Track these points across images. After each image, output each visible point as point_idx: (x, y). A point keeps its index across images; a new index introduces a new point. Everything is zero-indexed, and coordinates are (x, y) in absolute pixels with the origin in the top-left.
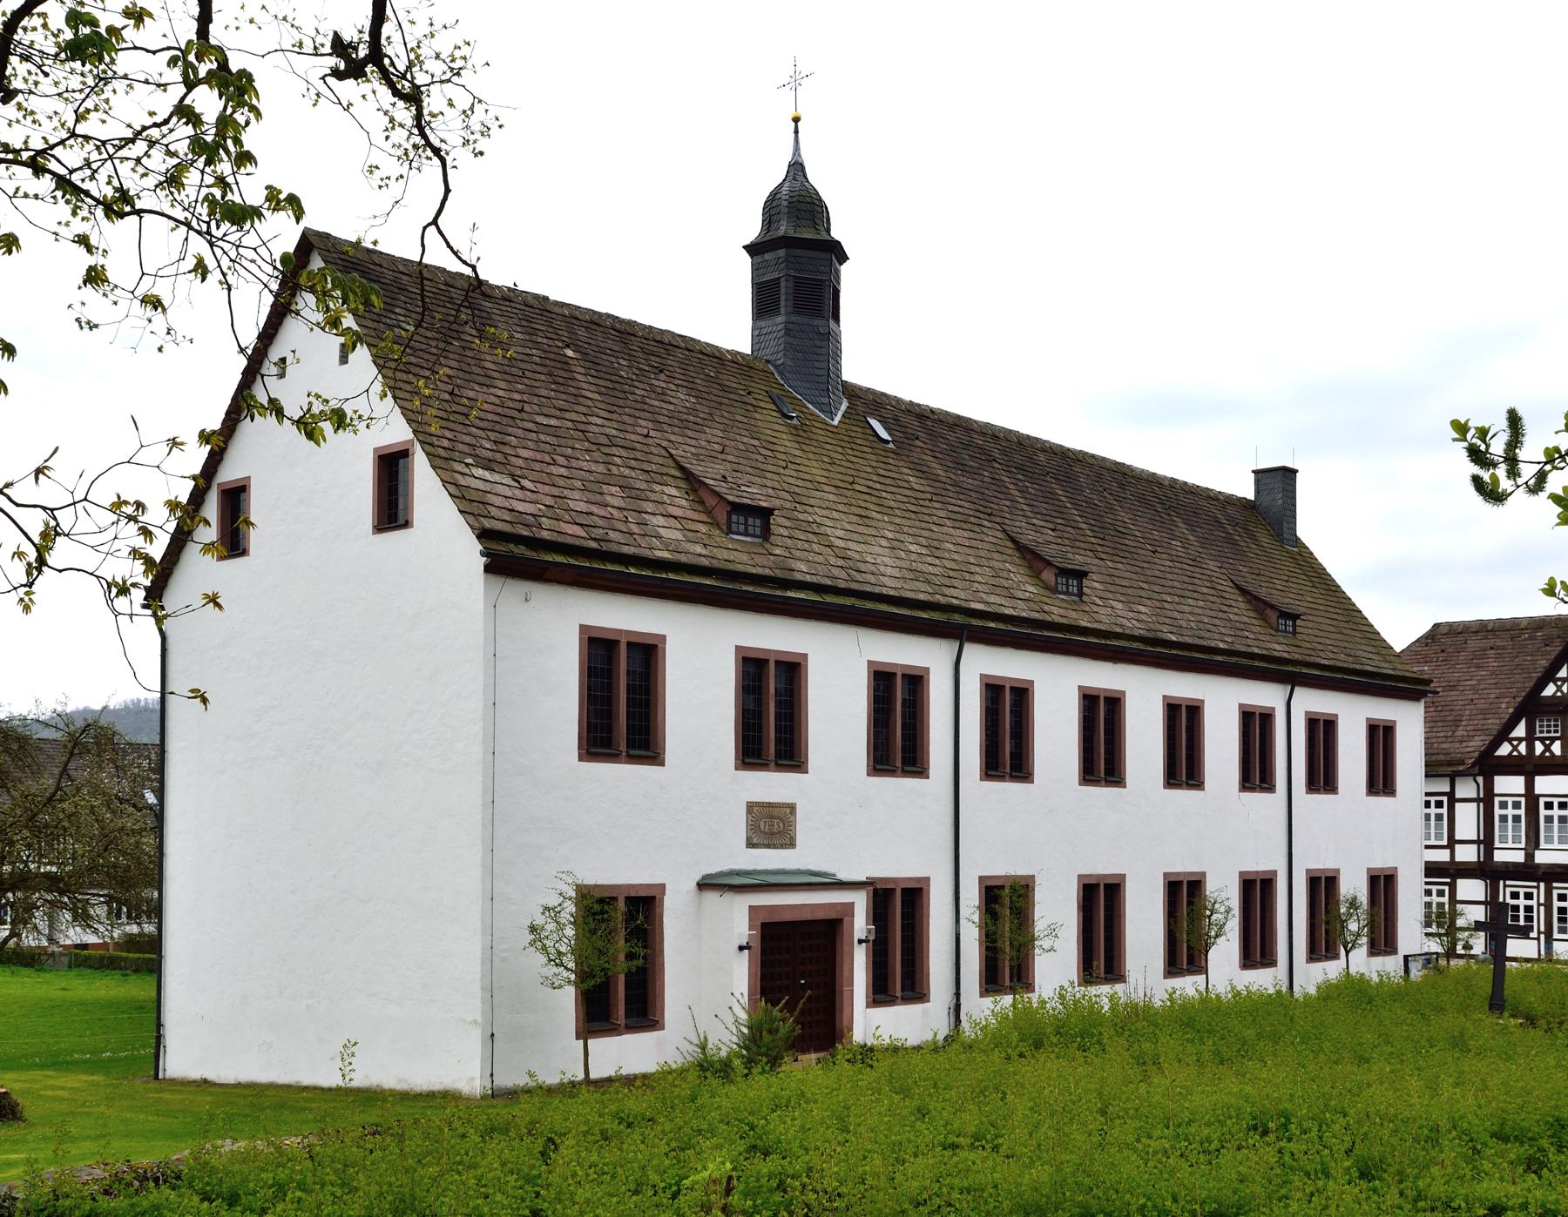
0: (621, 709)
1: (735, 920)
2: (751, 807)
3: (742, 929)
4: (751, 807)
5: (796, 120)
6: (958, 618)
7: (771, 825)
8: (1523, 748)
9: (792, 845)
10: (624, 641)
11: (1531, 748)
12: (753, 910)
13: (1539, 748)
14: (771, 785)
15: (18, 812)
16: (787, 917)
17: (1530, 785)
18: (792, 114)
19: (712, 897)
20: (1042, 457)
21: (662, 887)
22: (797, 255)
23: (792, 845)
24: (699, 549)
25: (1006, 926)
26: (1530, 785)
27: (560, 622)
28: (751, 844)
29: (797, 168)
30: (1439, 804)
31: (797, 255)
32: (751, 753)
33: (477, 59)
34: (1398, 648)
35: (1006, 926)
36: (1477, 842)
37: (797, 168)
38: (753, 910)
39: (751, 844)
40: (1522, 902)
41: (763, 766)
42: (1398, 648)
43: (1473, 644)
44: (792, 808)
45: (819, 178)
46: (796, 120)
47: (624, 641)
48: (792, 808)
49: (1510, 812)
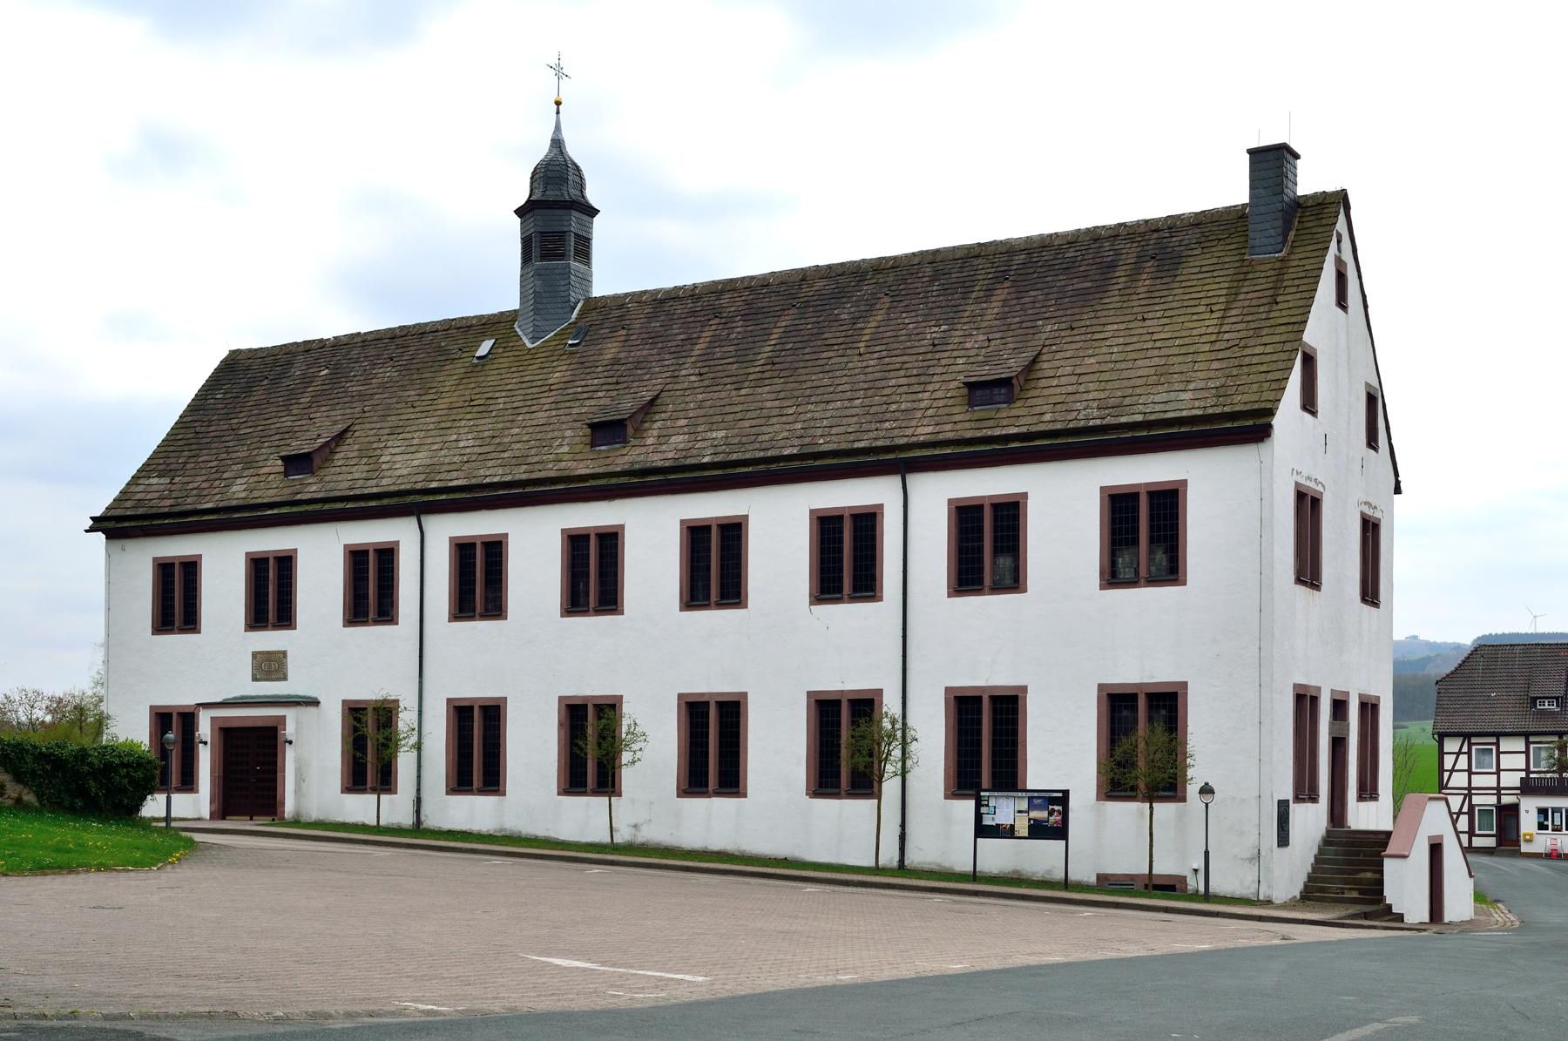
0: (176, 602)
2: (255, 655)
4: (255, 655)
5: (558, 103)
6: (409, 499)
7: (270, 666)
9: (285, 679)
10: (847, 514)
14: (270, 640)
16: (260, 724)
17: (1499, 800)
18: (554, 97)
22: (556, 213)
23: (285, 679)
25: (1370, 534)
26: (1499, 800)
27: (144, 556)
28: (255, 679)
29: (557, 143)
31: (556, 213)
34: (1247, 201)
35: (1370, 534)
36: (168, 819)
37: (557, 143)
39: (255, 679)
42: (1247, 201)
44: (284, 653)
46: (558, 103)
47: (847, 514)
48: (284, 653)
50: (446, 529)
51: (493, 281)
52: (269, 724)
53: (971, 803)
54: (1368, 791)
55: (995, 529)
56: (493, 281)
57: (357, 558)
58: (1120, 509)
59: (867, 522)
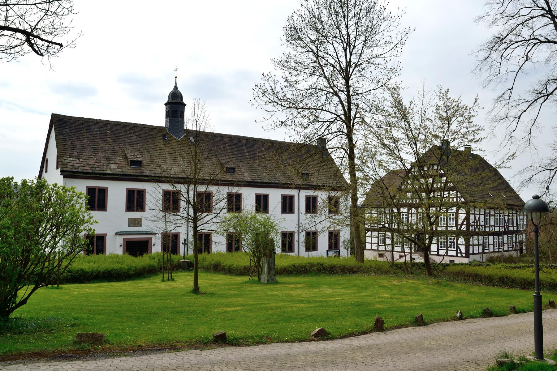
1: (120, 240)
3: (121, 242)
5: (176, 78)
6: (149, 178)
8: (455, 200)
11: (457, 200)
12: (124, 238)
13: (451, 200)
15: (415, 227)
16: (133, 240)
19: (118, 236)
20: (245, 141)
21: (106, 234)
22: (175, 105)
24: (120, 170)
28: (129, 226)
29: (176, 87)
30: (406, 215)
31: (175, 105)
32: (130, 207)
33: (531, 88)
37: (176, 87)
38: (124, 238)
39: (129, 226)
40: (443, 240)
41: (287, 213)
43: (486, 174)
45: (180, 89)
46: (176, 78)
49: (452, 217)
50: (304, 193)
51: (158, 118)
52: (146, 240)
53: (193, 274)
54: (444, 242)
55: (95, 197)
56: (158, 118)
57: (284, 197)
58: (130, 193)
59: (291, 198)
